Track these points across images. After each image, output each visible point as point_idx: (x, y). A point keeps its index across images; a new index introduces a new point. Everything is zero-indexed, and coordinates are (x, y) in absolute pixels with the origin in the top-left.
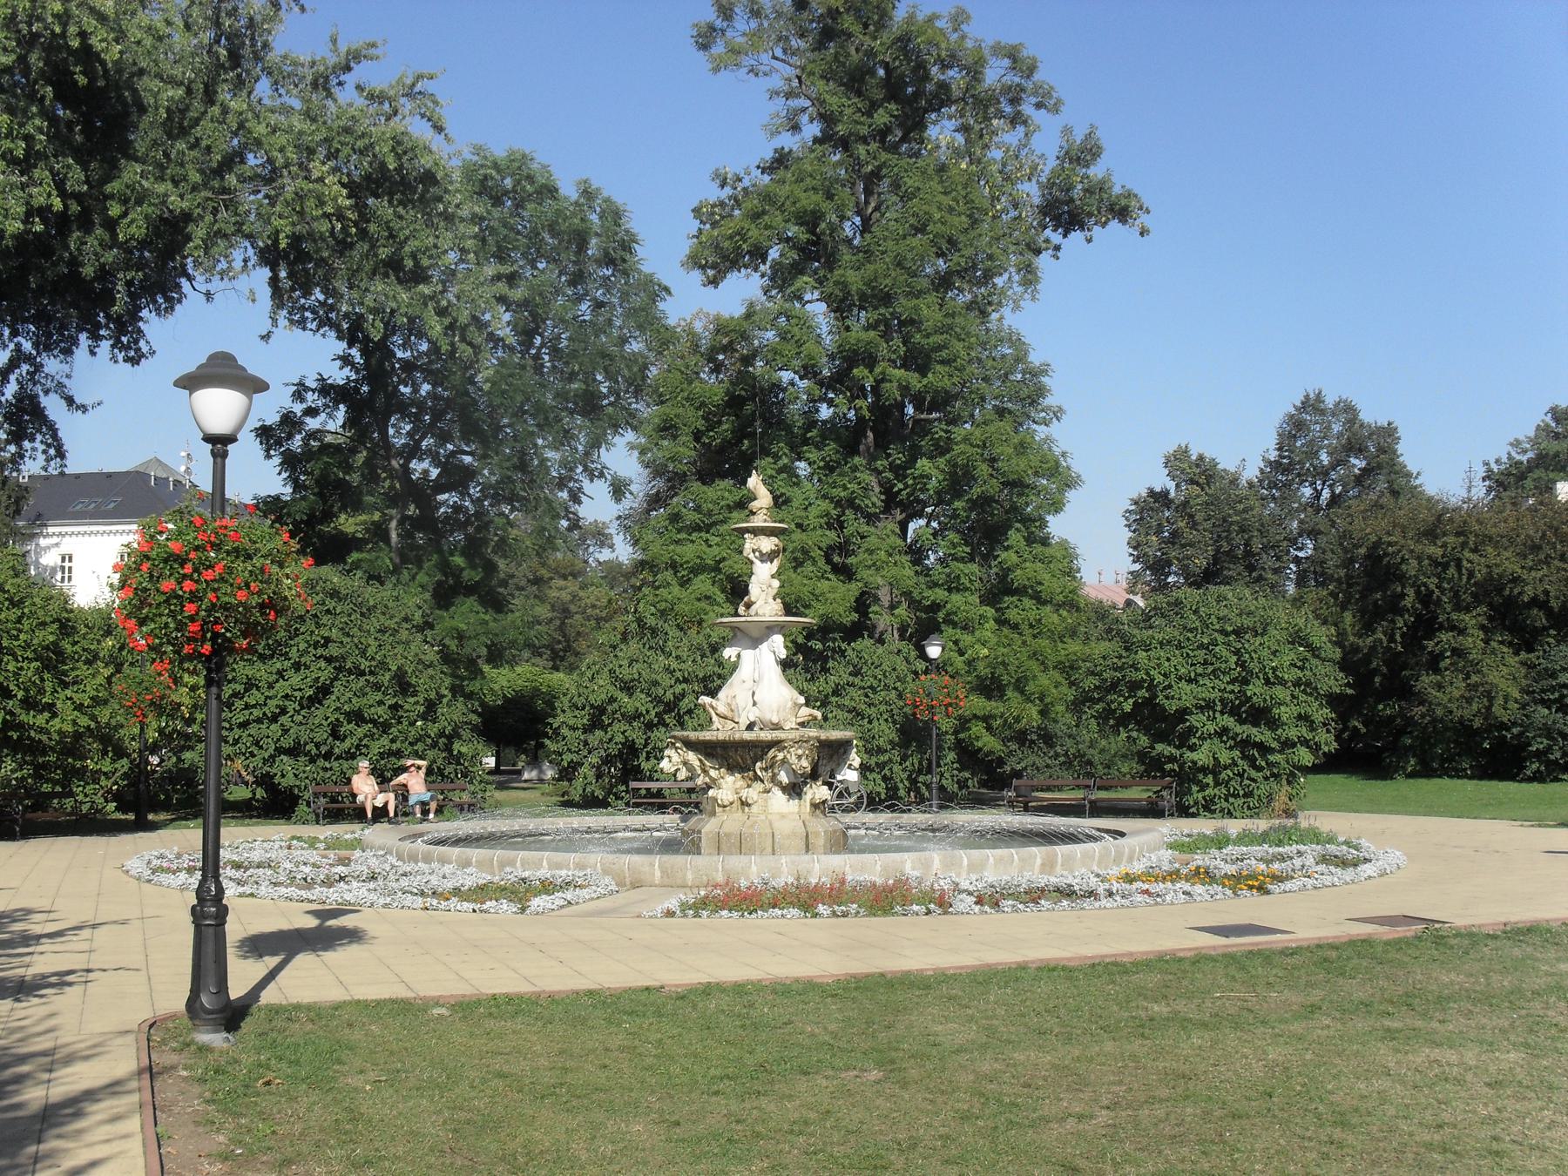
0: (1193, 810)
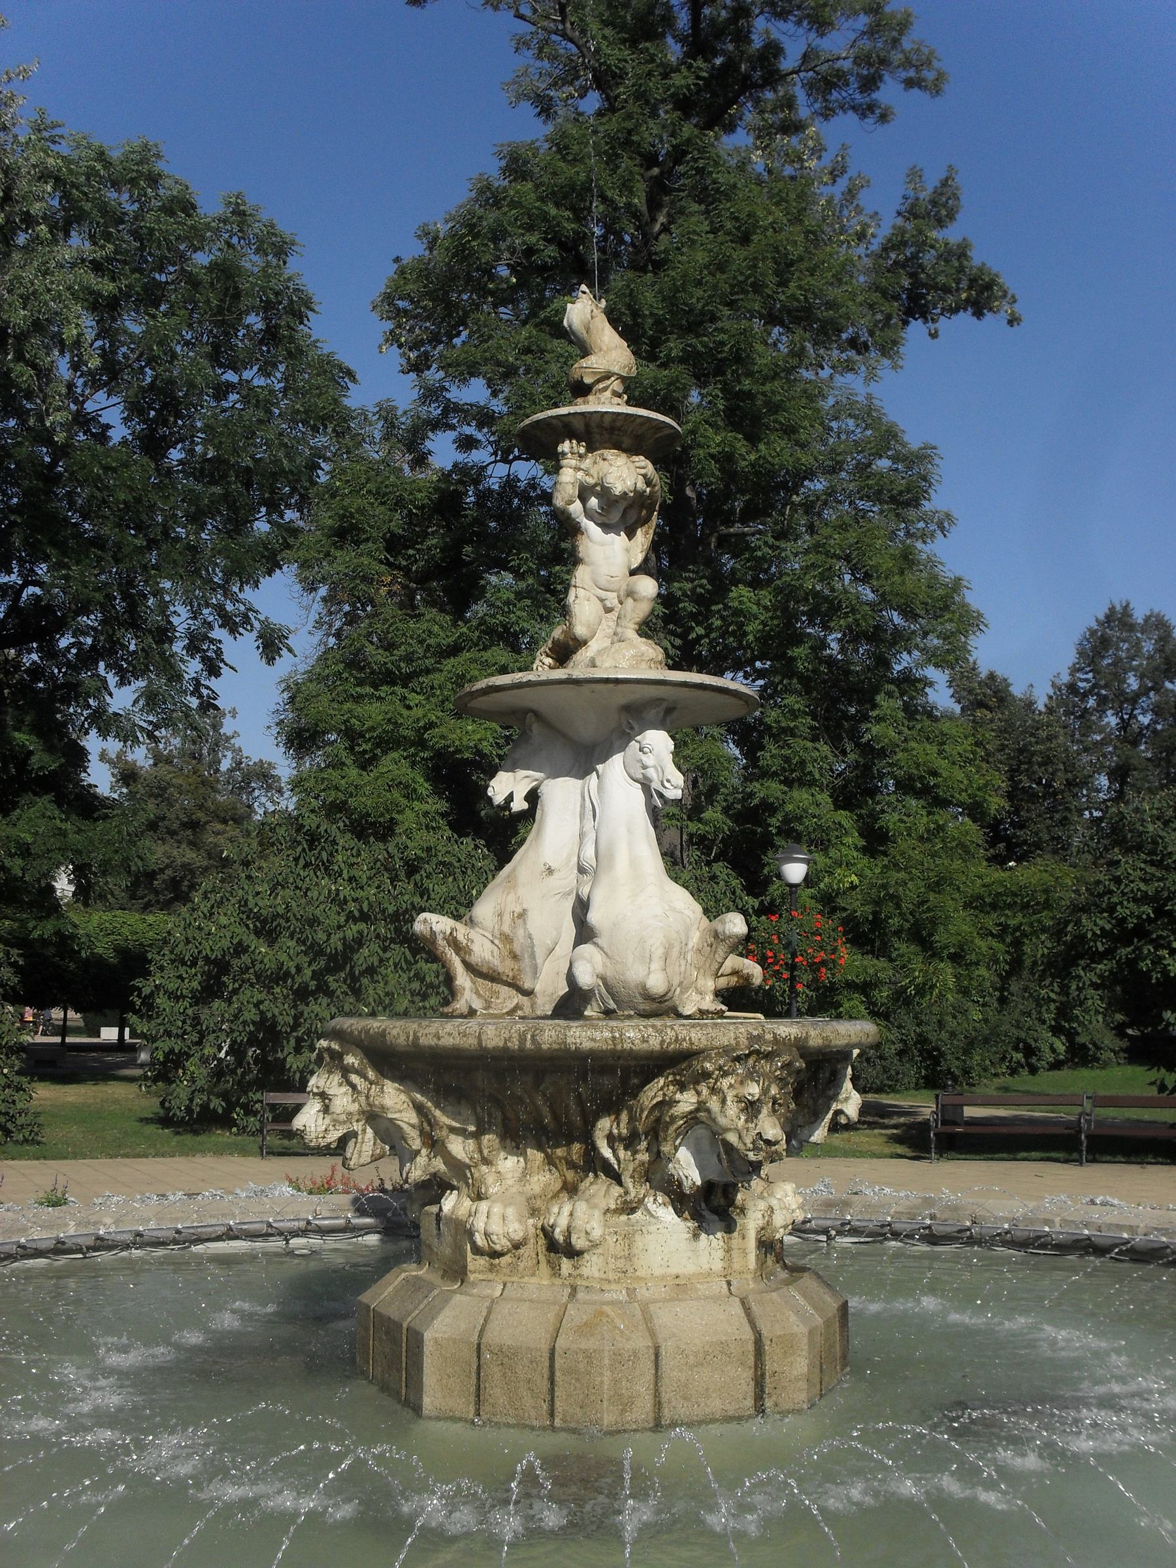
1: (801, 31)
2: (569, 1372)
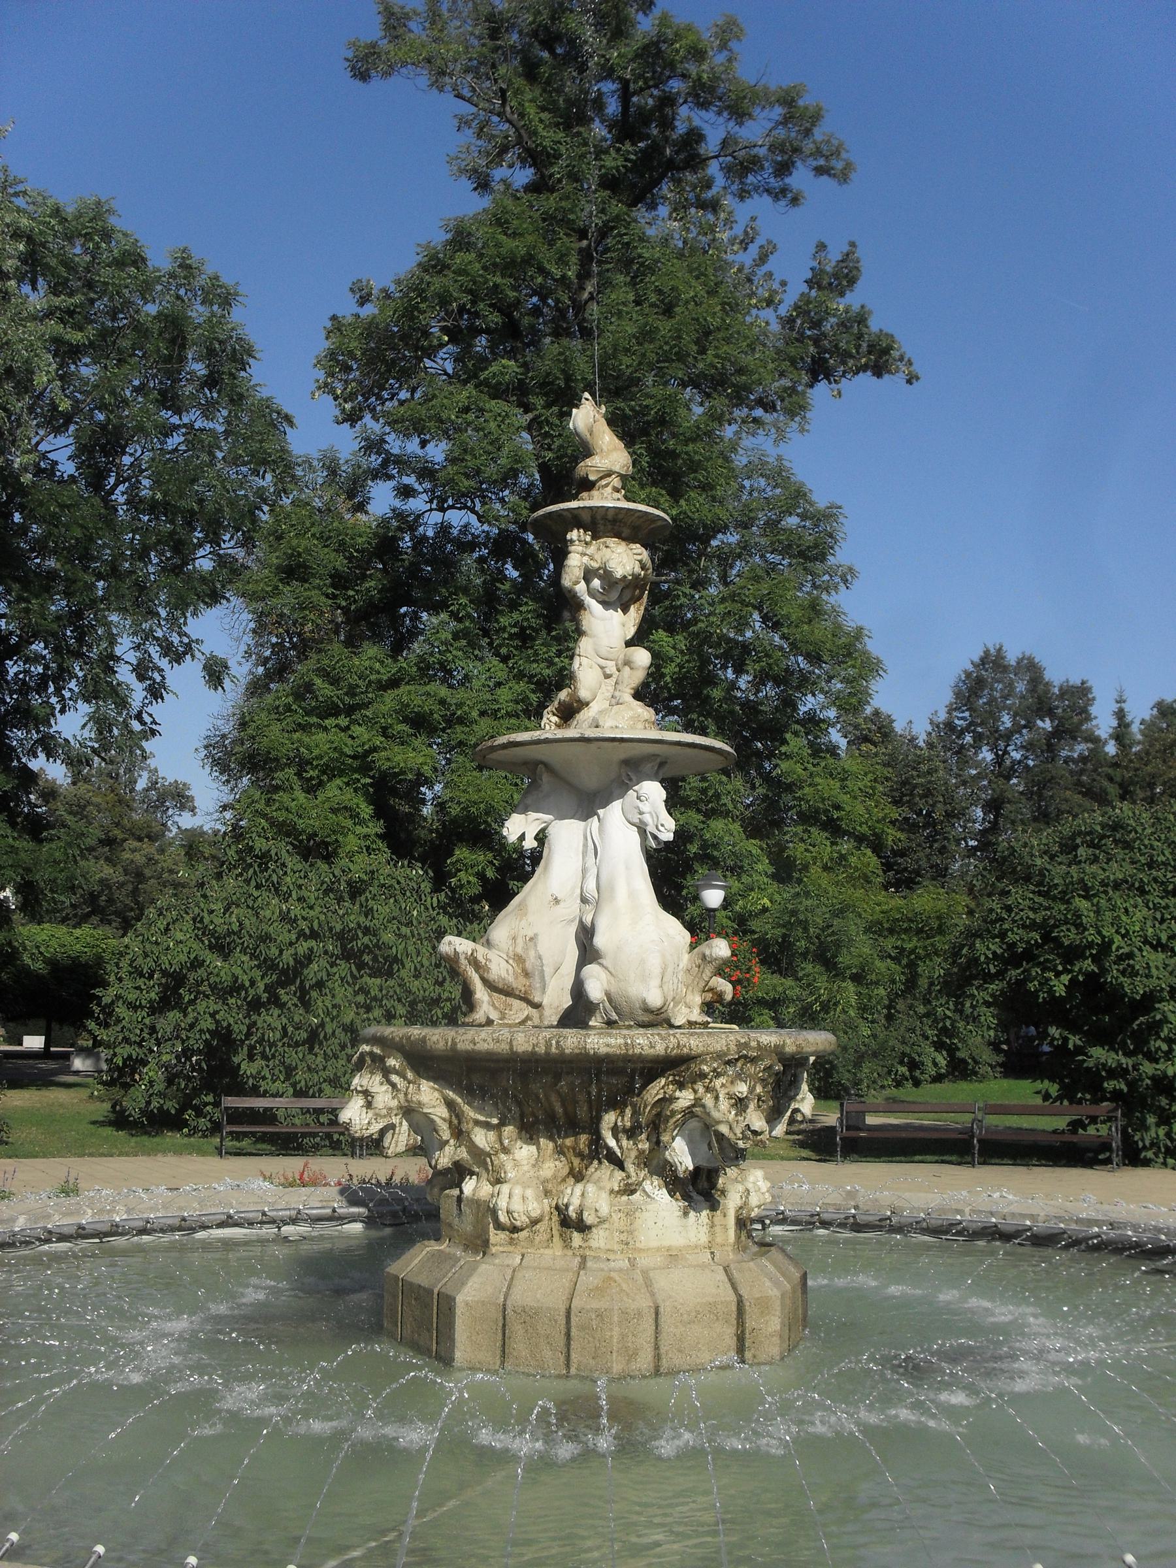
0: (1150, 1154)
1: (721, 120)
2: (582, 1328)
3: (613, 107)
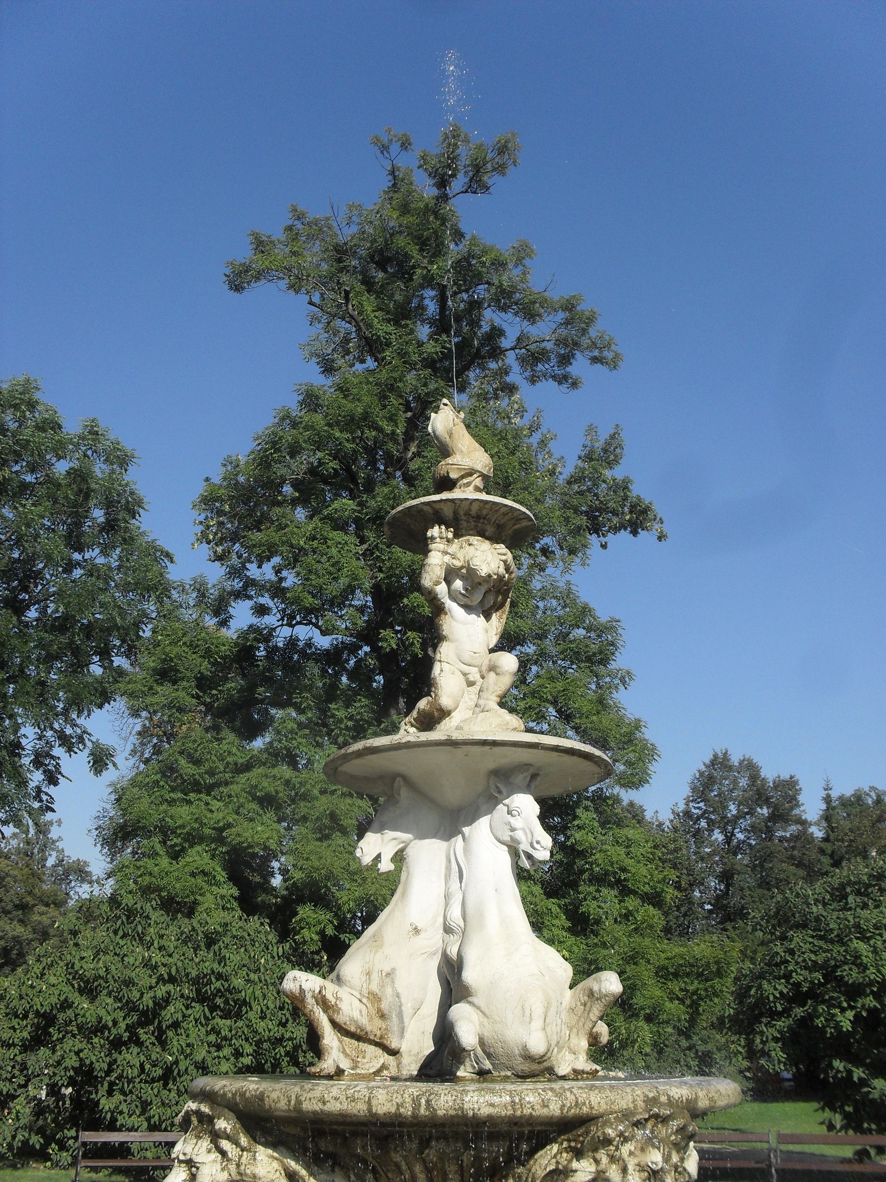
3: (432, 307)
